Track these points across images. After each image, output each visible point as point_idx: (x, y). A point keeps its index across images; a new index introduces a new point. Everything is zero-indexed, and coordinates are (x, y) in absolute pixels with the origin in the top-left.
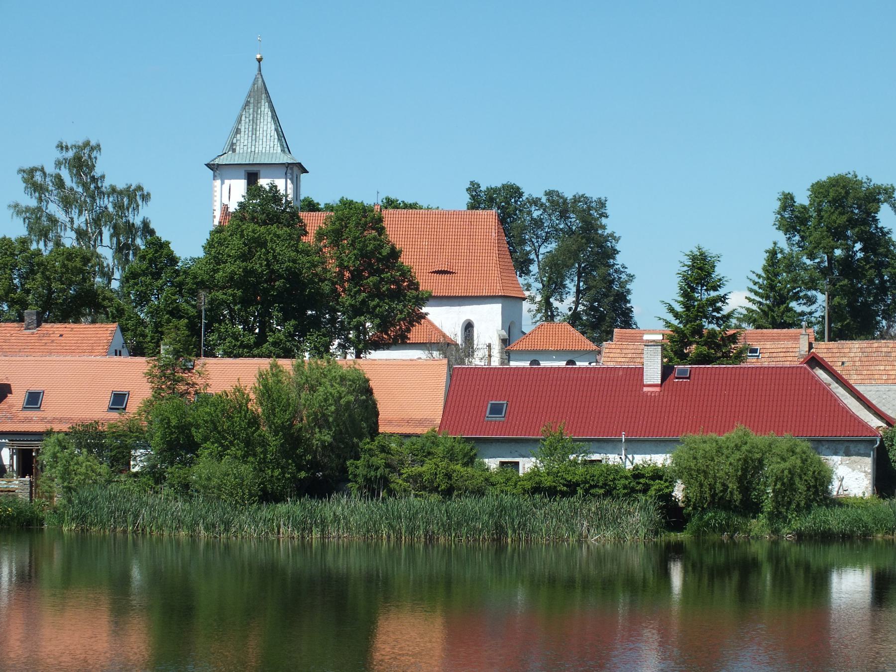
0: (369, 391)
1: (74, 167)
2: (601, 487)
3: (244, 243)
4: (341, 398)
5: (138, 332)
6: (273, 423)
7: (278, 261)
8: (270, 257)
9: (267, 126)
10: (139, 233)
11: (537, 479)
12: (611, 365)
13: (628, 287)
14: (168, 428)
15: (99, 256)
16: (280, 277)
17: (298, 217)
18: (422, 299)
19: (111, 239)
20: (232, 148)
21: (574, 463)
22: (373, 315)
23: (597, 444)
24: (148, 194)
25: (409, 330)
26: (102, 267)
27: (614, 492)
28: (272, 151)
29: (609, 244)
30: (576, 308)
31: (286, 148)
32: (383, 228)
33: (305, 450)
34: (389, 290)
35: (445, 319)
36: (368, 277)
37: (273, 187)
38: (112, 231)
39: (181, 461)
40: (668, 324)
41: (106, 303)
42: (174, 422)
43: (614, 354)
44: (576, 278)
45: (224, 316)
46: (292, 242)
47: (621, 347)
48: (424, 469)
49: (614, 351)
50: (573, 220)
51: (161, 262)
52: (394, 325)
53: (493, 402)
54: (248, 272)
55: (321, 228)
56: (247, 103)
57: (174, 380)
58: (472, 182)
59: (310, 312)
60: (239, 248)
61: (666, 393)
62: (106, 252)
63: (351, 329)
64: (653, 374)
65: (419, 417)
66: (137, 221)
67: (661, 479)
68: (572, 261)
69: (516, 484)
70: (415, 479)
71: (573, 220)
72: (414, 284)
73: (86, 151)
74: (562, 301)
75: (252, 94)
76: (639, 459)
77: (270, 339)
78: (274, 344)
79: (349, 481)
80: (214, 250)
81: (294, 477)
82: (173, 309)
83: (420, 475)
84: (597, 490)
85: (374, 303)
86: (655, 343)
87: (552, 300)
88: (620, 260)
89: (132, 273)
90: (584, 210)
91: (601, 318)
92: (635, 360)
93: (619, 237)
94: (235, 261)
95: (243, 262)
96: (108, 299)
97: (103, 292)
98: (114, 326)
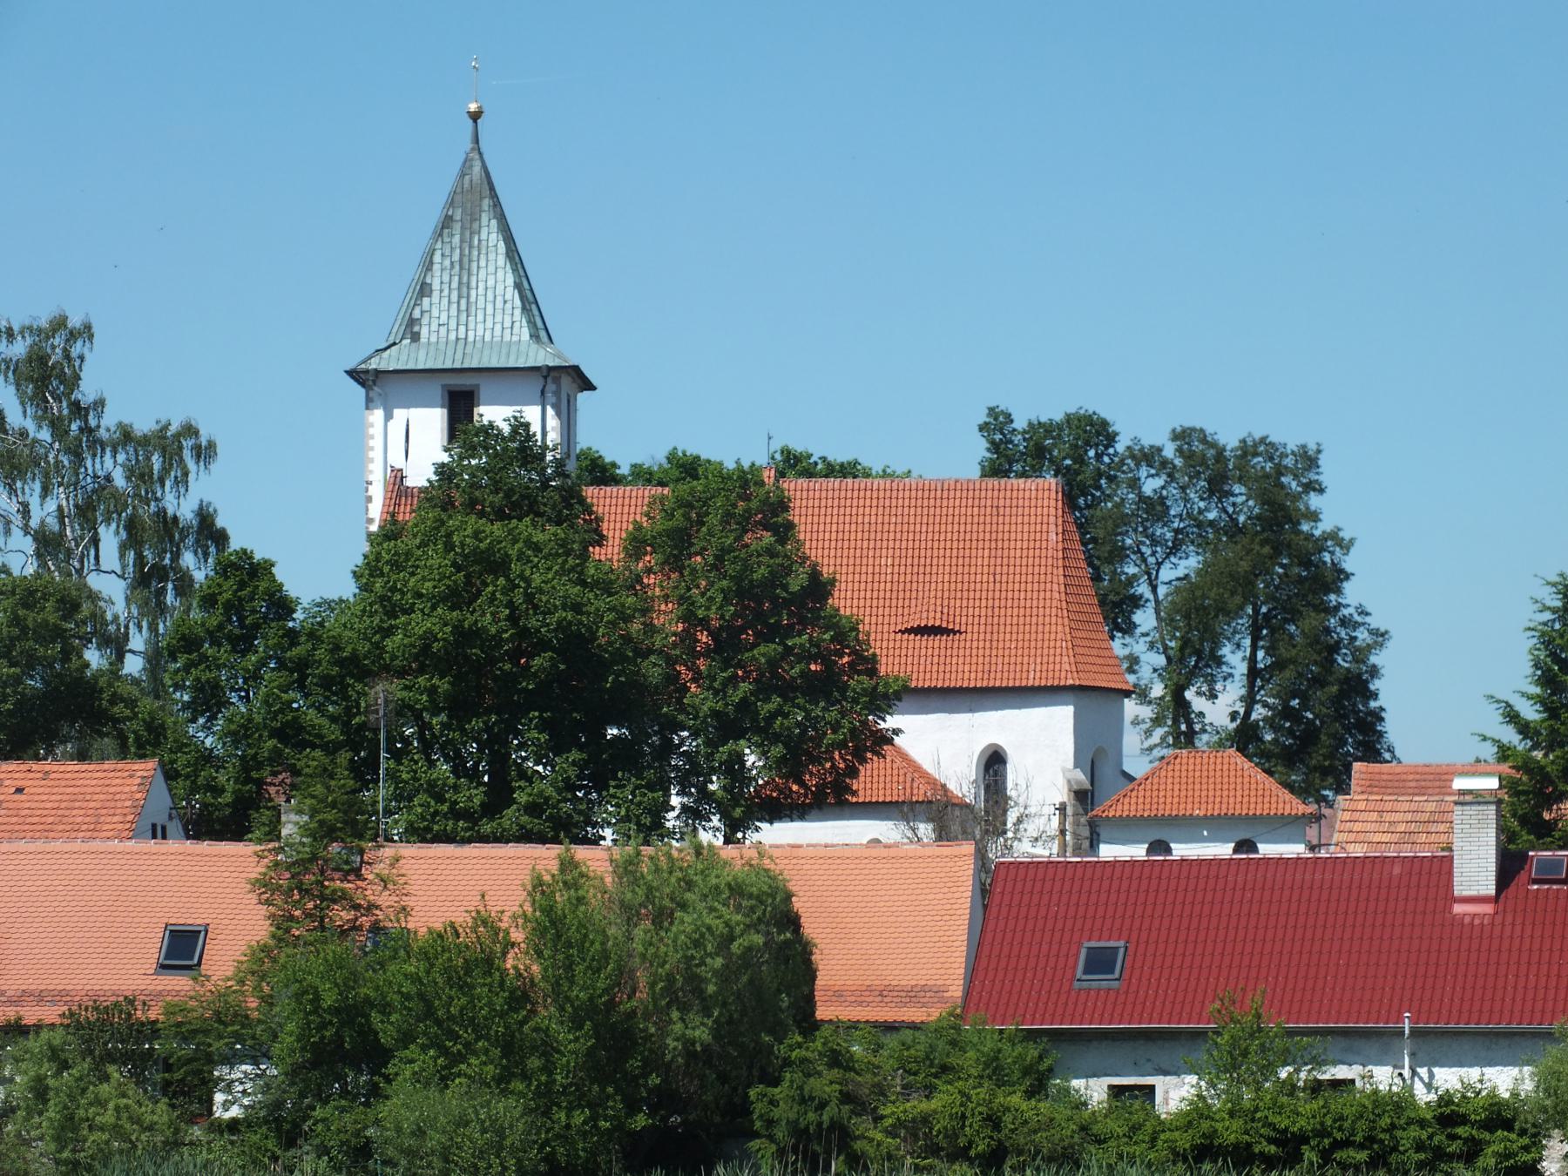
0: (791, 921)
1: (30, 379)
2: (1362, 1147)
3: (454, 564)
4: (732, 939)
5: (200, 781)
6: (567, 998)
7: (536, 607)
8: (519, 599)
9: (494, 276)
10: (190, 541)
11: (1205, 1125)
12: (1357, 851)
13: (1373, 659)
14: (315, 1011)
15: (94, 597)
16: (544, 645)
17: (582, 501)
18: (885, 696)
19: (122, 556)
20: (411, 329)
21: (1290, 1087)
22: (765, 735)
23: (1342, 1042)
24: (211, 445)
25: (853, 772)
26: (97, 617)
27: (1393, 1159)
28: (507, 337)
29: (1327, 557)
30: (1248, 713)
31: (540, 331)
32: (790, 526)
33: (646, 1062)
34: (805, 674)
35: (938, 745)
36: (754, 646)
37: (520, 427)
38: (124, 535)
39: (344, 1093)
40: (1504, 753)
41: (119, 710)
42: (329, 999)
43: (1361, 826)
44: (1247, 642)
45: (406, 741)
46: (571, 561)
47: (1380, 806)
48: (935, 1104)
49: (1364, 816)
50: (1240, 499)
51: (254, 611)
52: (817, 760)
53: (1093, 944)
54: (466, 636)
55: (638, 527)
56: (447, 222)
57: (323, 898)
58: (992, 411)
59: (612, 731)
60: (443, 577)
61: (1509, 919)
62: (110, 585)
63: (713, 771)
64: (1475, 870)
65: (906, 981)
66: (184, 509)
67: (1510, 1128)
68: (1238, 599)
69: (1154, 1140)
70: (914, 1129)
71: (1240, 499)
72: (866, 660)
73: (58, 340)
74: (1213, 696)
75: (458, 198)
76: (1449, 1078)
77: (521, 798)
78: (533, 809)
79: (756, 1135)
80: (379, 584)
81: (619, 1127)
82: (285, 725)
83: (925, 1119)
84: (1352, 1152)
85: (771, 706)
86: (1475, 798)
87: (1189, 694)
88: (1352, 594)
89: (183, 638)
90: (1267, 476)
91: (1308, 737)
92: (1414, 838)
93: (1352, 541)
94: (434, 608)
95: (452, 609)
96: (122, 700)
97: (110, 685)
98: (147, 768)
